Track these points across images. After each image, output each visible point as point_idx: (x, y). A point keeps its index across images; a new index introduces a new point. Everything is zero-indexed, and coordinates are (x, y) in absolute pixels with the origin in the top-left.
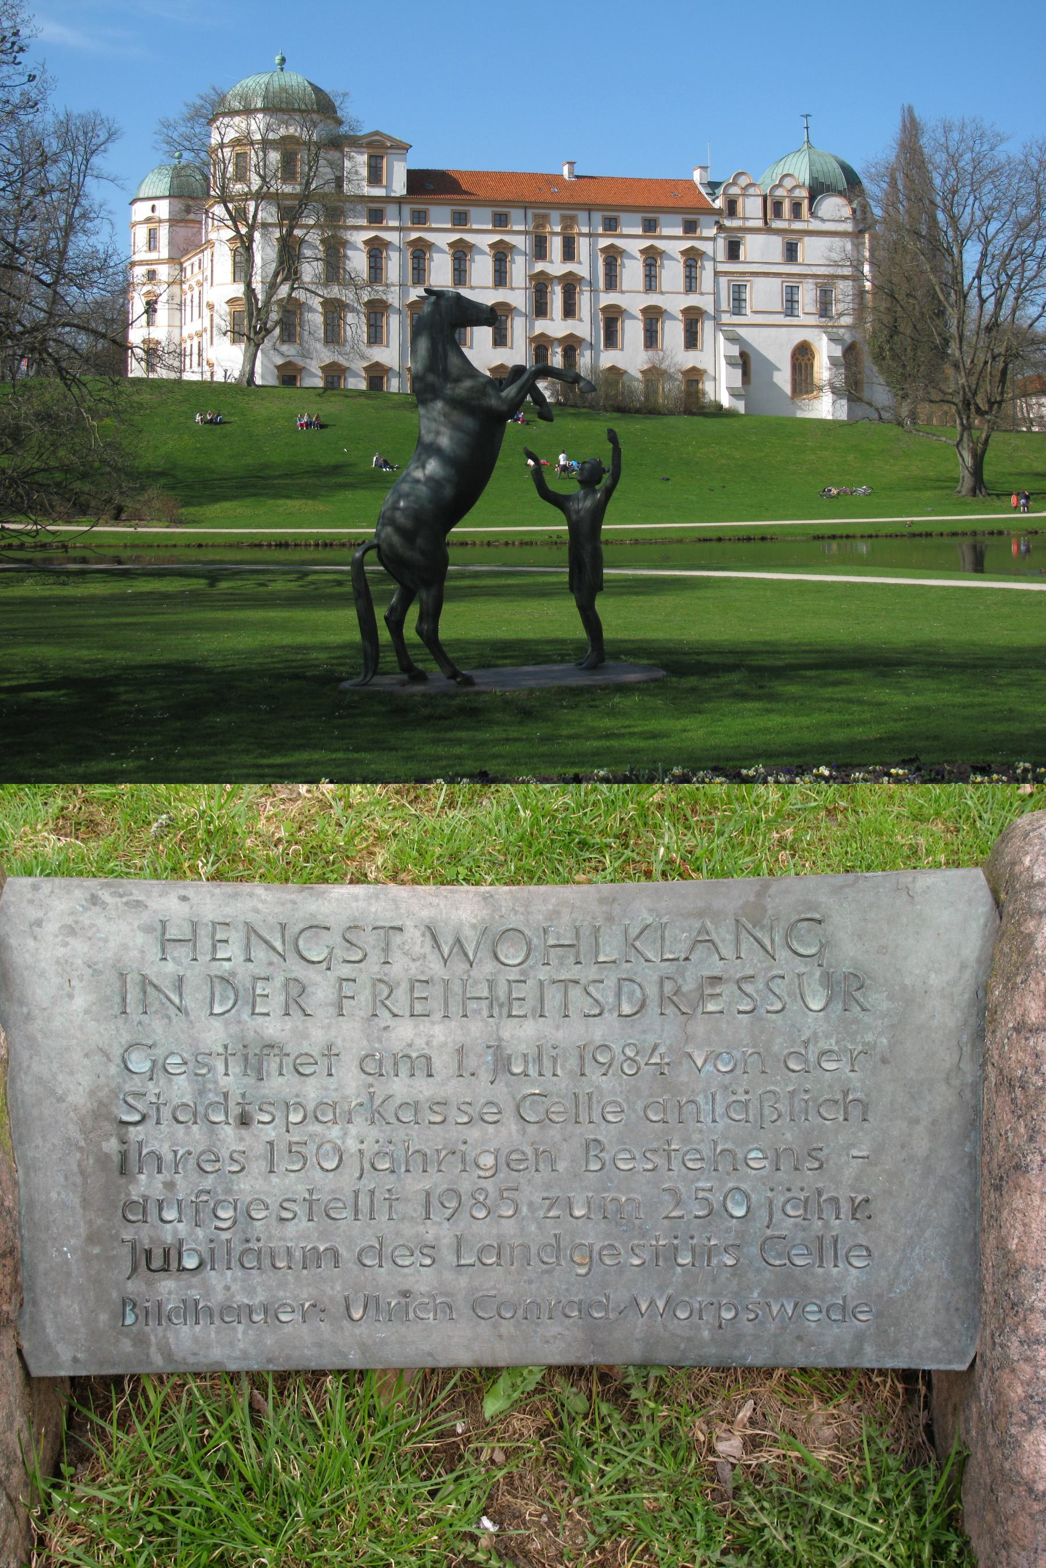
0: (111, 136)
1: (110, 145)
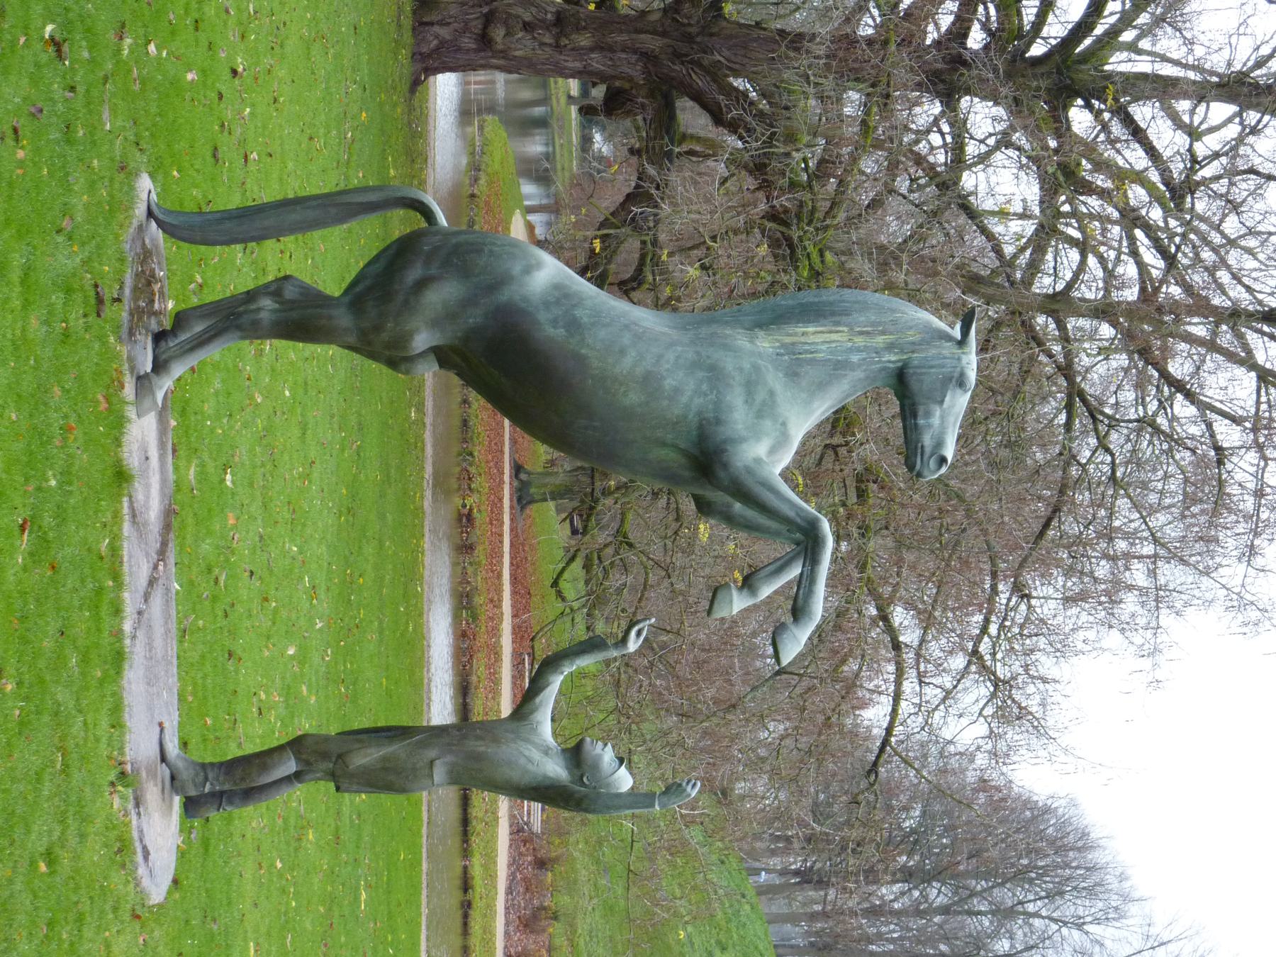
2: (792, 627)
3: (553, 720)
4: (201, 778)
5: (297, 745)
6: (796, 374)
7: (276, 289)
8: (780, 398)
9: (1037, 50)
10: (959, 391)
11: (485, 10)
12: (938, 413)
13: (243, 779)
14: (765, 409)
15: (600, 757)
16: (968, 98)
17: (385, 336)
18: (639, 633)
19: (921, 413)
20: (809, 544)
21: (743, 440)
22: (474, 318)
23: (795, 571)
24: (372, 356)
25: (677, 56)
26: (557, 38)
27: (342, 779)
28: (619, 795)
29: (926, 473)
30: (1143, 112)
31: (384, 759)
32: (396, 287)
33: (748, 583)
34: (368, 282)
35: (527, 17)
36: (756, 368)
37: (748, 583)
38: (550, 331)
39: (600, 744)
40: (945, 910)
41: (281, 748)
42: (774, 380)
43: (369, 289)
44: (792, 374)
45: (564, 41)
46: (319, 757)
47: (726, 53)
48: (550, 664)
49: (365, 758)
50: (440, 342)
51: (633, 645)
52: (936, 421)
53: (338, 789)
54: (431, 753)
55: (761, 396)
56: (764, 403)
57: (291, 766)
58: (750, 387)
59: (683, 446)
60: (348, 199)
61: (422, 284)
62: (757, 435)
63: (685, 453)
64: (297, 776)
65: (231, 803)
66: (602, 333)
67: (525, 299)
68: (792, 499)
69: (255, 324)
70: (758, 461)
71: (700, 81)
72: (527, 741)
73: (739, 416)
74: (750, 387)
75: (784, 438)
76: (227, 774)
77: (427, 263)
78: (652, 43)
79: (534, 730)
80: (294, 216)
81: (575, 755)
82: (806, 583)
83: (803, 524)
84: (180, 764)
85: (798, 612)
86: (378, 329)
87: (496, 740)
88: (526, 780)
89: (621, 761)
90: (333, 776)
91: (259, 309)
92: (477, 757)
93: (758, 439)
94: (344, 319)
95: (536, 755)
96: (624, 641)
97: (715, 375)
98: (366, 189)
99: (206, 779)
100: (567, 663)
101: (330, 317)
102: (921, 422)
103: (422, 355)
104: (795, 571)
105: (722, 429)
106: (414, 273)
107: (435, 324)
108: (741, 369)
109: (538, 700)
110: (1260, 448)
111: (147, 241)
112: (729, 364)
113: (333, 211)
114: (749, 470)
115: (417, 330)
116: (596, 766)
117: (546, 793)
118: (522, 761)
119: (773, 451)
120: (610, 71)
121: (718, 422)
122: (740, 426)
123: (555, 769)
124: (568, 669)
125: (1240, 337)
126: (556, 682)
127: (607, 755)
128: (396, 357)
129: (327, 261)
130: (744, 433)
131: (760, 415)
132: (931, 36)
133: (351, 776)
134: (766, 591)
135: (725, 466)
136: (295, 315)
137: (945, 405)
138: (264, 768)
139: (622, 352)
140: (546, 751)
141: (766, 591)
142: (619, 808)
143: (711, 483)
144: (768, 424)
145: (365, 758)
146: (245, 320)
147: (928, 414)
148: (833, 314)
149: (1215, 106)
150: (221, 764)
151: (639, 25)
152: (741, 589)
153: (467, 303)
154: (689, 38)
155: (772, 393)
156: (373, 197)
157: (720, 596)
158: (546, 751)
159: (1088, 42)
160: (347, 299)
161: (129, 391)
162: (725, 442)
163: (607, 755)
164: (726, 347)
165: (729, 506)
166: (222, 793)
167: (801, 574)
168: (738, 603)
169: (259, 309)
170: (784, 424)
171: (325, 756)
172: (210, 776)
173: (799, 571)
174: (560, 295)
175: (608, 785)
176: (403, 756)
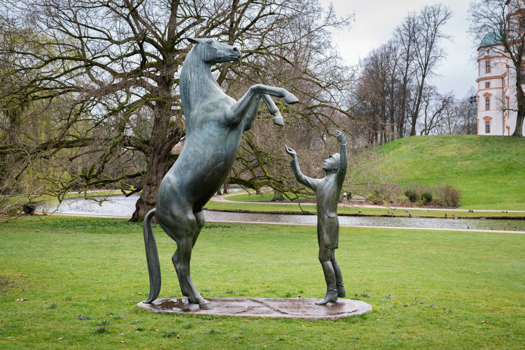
0: (447, 15)
1: (447, 21)
2: (286, 98)
3: (314, 178)
4: (332, 292)
5: (322, 261)
6: (205, 96)
7: (175, 261)
8: (213, 101)
9: (161, 57)
10: (213, 44)
11: (145, 204)
12: (219, 51)
13: (333, 278)
14: (216, 106)
15: (329, 163)
16: (175, 77)
17: (189, 228)
18: (290, 150)
19: (219, 56)
20: (260, 92)
21: (225, 113)
22: (183, 199)
23: (269, 97)
24: (198, 233)
25: (159, 154)
26: (153, 185)
27: (334, 246)
28: (341, 156)
29: (239, 55)
30: (179, 29)
31: (327, 232)
32: (173, 224)
33: (273, 113)
34: (172, 234)
35: (148, 193)
36: (203, 109)
37: (273, 113)
38: (189, 176)
39: (325, 163)
40: (392, 96)
41: (323, 265)
42: (207, 103)
43: (174, 233)
44: (205, 97)
45: (155, 183)
46: (326, 253)
47: (159, 140)
48: (299, 179)
49: (326, 238)
50: (192, 212)
51: (294, 152)
52: (222, 51)
53: (337, 248)
54: (326, 217)
55: (212, 108)
56: (214, 106)
57: (329, 263)
58: (208, 111)
59: (227, 133)
60: (147, 239)
61: (173, 216)
62: (223, 108)
63: (229, 133)
64: (333, 261)
65: (341, 282)
66: (190, 158)
67: (178, 183)
68: (245, 96)
69: (184, 270)
70: (232, 108)
71: (166, 147)
72: (323, 187)
73: (218, 114)
74: (208, 111)
75: (226, 100)
76: (331, 284)
77: (167, 214)
78: (156, 160)
79: (320, 184)
80: (152, 256)
81: (328, 171)
82: (273, 94)
83: (253, 93)
84: (327, 298)
85: (281, 96)
86: (187, 231)
87: (323, 197)
88: (336, 187)
89: (331, 156)
90: (333, 250)
91: (180, 269)
92: (328, 202)
93: (226, 108)
94: (184, 241)
95: (328, 184)
96: (292, 155)
97: (204, 121)
98: (144, 233)
99: (332, 290)
100: (299, 173)
101: (183, 246)
102: (222, 56)
103: (197, 217)
104: (269, 97)
105: (221, 120)
106: (169, 218)
107: (185, 212)
108: (203, 113)
109: (310, 183)
110: (271, 4)
111: (158, 304)
112: (201, 117)
113: (150, 244)
114: (235, 111)
115: (187, 218)
116: (332, 165)
117: (340, 180)
118: (330, 188)
119: (229, 103)
120: (163, 172)
121: (219, 121)
122: (221, 114)
123: (332, 178)
124: (300, 173)
125: (241, 6)
126: (304, 177)
127: (329, 161)
128: (199, 225)
129: (166, 247)
130: (223, 113)
131: (217, 107)
132: (156, 85)
133: (332, 243)
134: (276, 107)
135: (233, 119)
136: (182, 257)
137: (217, 48)
138: (329, 271)
139: (196, 151)
140: (327, 180)
141: (276, 107)
142: (345, 157)
143: (239, 123)
144: (220, 105)
145: (326, 238)
146: (183, 274)
147: (220, 54)
148: (187, 84)
149: (178, 12)
150: (327, 285)
151: (151, 163)
152: (275, 115)
153: (179, 202)
154: (155, 150)
155: (211, 103)
156: (147, 231)
157: (276, 122)
158: (327, 180)
159: (159, 43)
160: (177, 240)
161: (203, 312)
162: (226, 119)
163: (329, 161)
164: (196, 118)
165: (248, 119)
166: (337, 285)
167: (270, 95)
168: (279, 117)
169: (180, 269)
170: (221, 100)
171: (326, 252)
172: (331, 289)
173: (269, 96)
174: (178, 173)
175: (338, 161)
176: (327, 226)
